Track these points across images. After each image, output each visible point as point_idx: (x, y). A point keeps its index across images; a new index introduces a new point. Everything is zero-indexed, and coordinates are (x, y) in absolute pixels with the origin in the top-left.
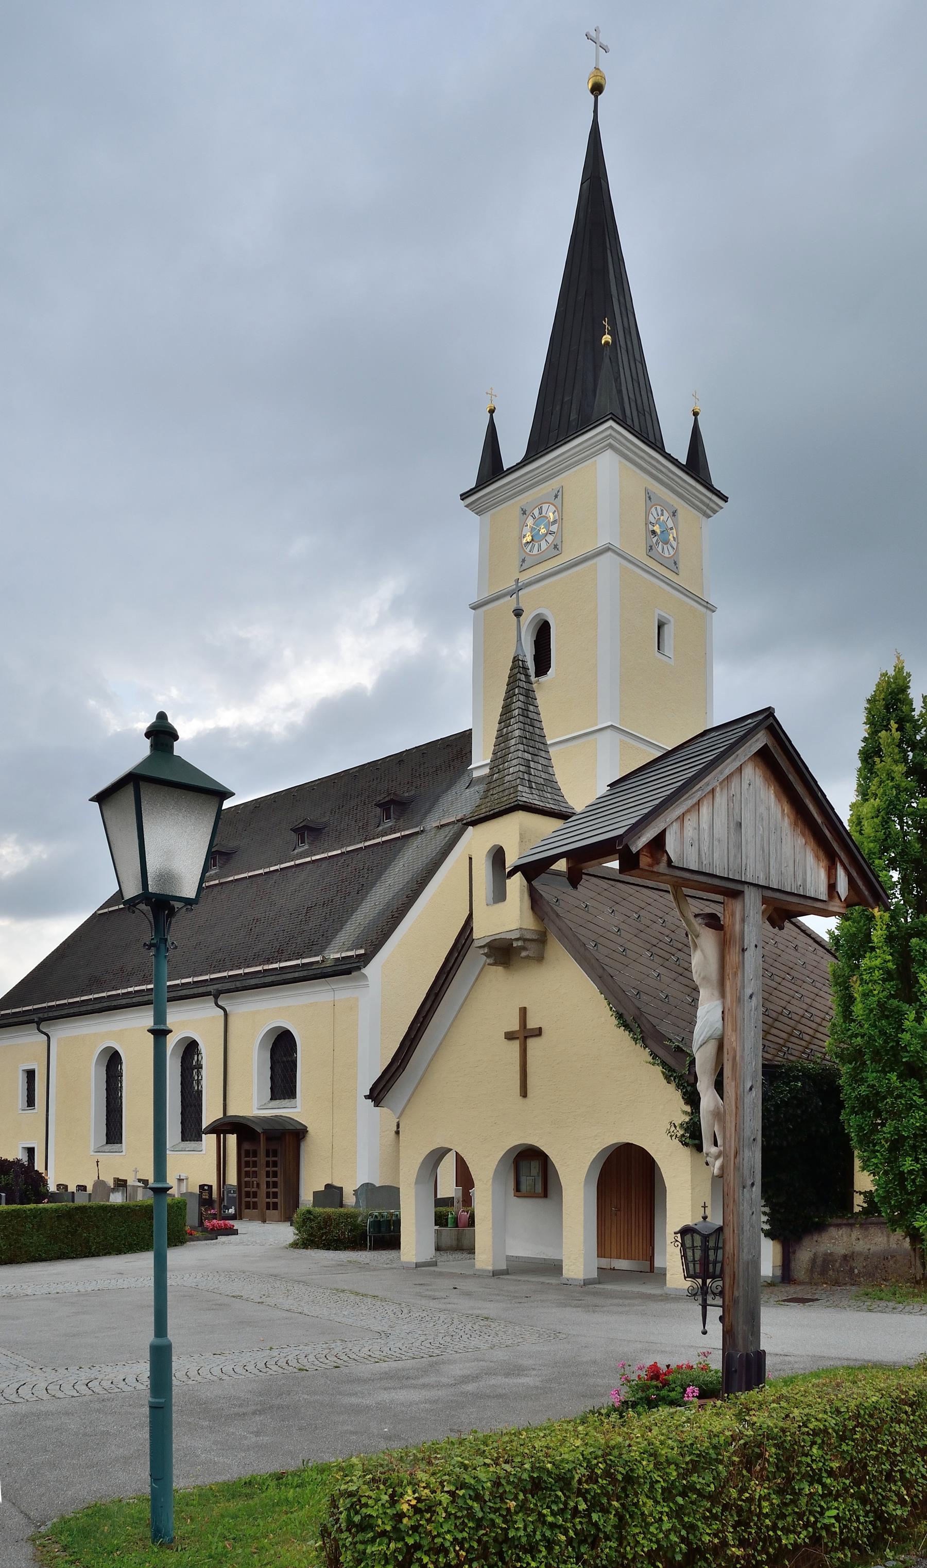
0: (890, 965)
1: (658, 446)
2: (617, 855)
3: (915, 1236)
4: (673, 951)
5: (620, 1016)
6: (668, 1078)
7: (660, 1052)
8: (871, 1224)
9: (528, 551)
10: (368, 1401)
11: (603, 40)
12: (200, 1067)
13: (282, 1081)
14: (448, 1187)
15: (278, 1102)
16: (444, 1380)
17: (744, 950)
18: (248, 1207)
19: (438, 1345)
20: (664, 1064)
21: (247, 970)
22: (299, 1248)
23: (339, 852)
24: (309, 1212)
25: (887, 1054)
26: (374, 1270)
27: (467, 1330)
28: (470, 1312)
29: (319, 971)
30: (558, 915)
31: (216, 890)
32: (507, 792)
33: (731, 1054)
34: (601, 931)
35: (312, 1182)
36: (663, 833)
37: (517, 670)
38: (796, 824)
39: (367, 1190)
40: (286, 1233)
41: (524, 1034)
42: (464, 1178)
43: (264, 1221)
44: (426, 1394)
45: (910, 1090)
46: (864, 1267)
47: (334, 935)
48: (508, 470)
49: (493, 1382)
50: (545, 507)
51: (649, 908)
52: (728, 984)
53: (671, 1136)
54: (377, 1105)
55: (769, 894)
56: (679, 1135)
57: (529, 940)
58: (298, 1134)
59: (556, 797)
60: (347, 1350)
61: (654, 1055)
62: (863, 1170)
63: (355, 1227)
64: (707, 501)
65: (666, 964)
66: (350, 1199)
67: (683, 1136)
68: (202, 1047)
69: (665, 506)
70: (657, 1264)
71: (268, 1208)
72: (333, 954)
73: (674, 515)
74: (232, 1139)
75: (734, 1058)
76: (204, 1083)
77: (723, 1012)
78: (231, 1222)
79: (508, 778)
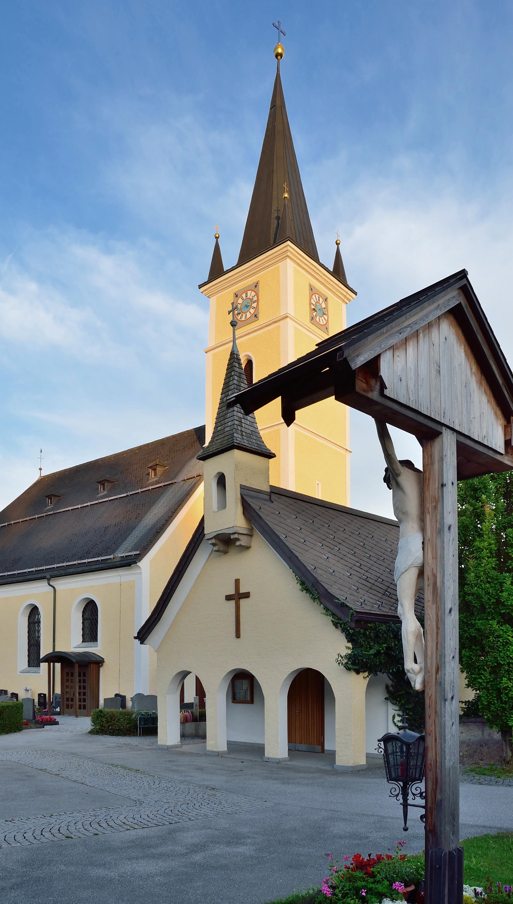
0: (493, 546)
1: (315, 258)
2: (332, 389)
3: (506, 731)
4: (336, 544)
5: (302, 583)
6: (336, 625)
7: (331, 607)
8: (470, 722)
9: (239, 318)
10: (112, 874)
11: (282, 28)
12: (39, 622)
13: (89, 631)
14: (190, 697)
15: (87, 643)
16: (178, 849)
17: (443, 485)
18: (68, 707)
19: (177, 812)
20: (333, 615)
21: (68, 564)
22: (95, 734)
23: (125, 495)
24: (101, 711)
25: (490, 608)
26: (140, 750)
27: (199, 799)
28: (202, 784)
29: (112, 564)
30: (260, 517)
31: (51, 517)
32: (226, 438)
33: (431, 581)
34: (289, 529)
35: (107, 691)
36: (377, 358)
37: (232, 360)
38: (481, 384)
39: (139, 697)
40: (86, 723)
41: (238, 596)
42: (200, 692)
43: (77, 716)
44: (162, 865)
45: (506, 632)
46: (467, 751)
47: (120, 544)
48: (227, 271)
49: (217, 851)
50: (249, 292)
51: (319, 517)
52: (428, 517)
53: (339, 663)
54: (142, 643)
55: (462, 439)
56: (344, 662)
57: (241, 534)
58: (98, 662)
59: (258, 442)
60: (109, 817)
61: (326, 609)
62: (468, 687)
63: (130, 721)
64: (345, 294)
65: (332, 551)
66: (129, 704)
67: (347, 663)
68: (41, 610)
69: (320, 295)
70: (327, 746)
71: (80, 708)
72: (120, 554)
73: (326, 301)
74: (58, 666)
75: (435, 583)
76: (42, 632)
77: (423, 543)
78: (55, 717)
79: (227, 429)
